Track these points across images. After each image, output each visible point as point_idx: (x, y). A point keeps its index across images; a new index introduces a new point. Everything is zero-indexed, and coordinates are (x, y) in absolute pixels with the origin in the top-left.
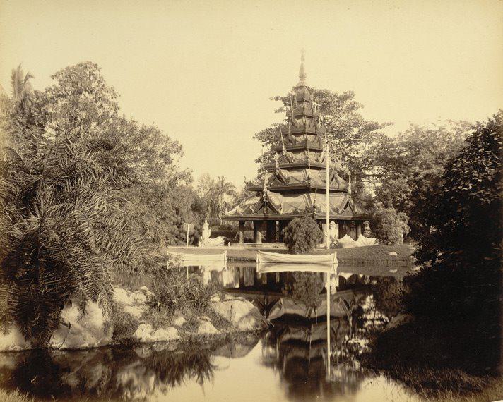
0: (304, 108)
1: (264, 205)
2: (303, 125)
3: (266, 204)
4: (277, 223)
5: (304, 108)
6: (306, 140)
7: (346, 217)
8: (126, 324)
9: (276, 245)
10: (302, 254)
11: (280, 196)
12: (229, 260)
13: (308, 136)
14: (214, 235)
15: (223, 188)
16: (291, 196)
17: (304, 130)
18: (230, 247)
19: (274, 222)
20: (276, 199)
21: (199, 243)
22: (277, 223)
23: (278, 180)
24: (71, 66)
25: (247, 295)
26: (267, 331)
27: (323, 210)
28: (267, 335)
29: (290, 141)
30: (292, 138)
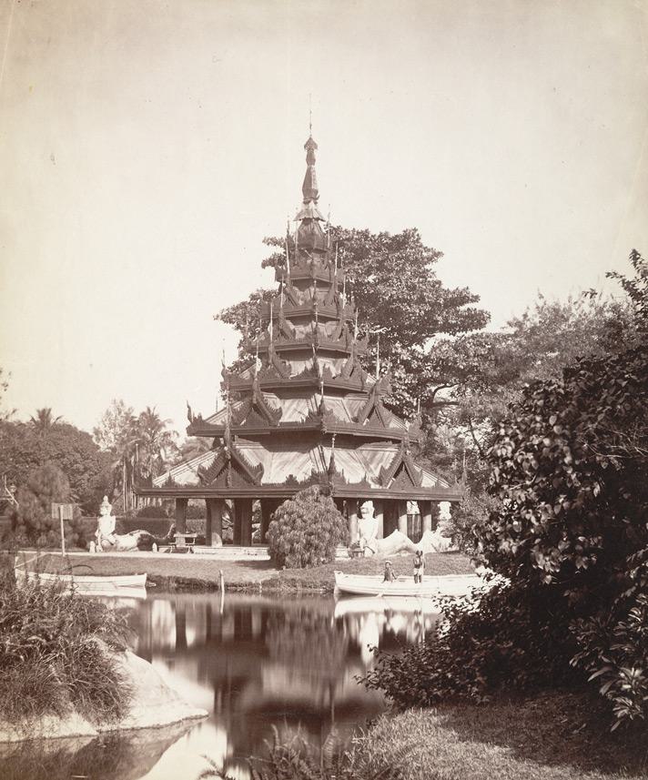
2: (346, 302)
3: (234, 463)
4: (257, 505)
7: (398, 494)
8: (578, 526)
9: (253, 550)
10: (191, 593)
11: (261, 449)
14: (124, 527)
16: (291, 450)
17: (312, 312)
18: (157, 553)
19: (250, 501)
20: (251, 454)
21: (92, 544)
22: (257, 505)
23: (255, 414)
24: (375, 231)
25: (168, 660)
29: (283, 333)
30: (288, 327)
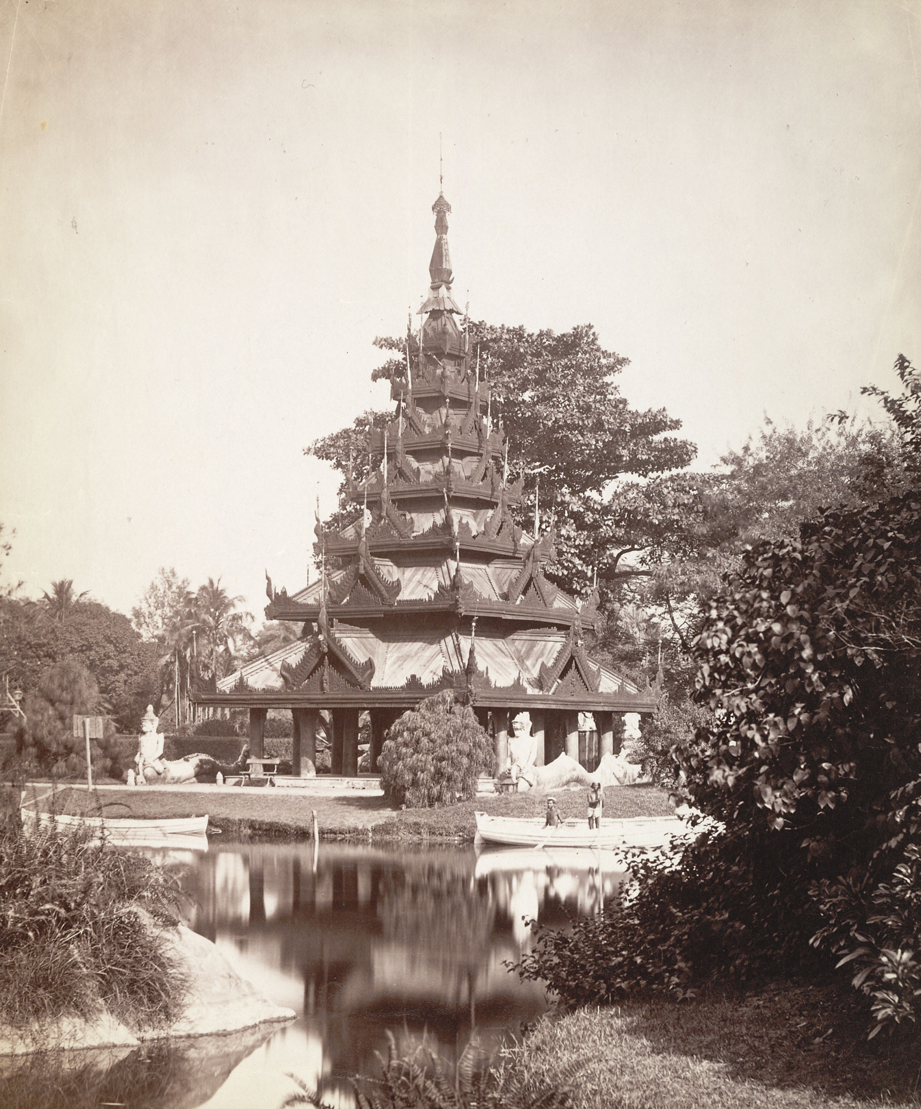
0: (443, 375)
1: (320, 663)
4: (365, 717)
5: (443, 375)
6: (448, 472)
7: (565, 702)
9: (359, 782)
11: (371, 639)
12: (210, 823)
13: (467, 568)
14: (177, 749)
15: (203, 610)
18: (223, 786)
20: (356, 645)
21: (131, 773)
22: (365, 717)
23: (363, 589)
25: (238, 938)
26: (766, 764)
27: (485, 596)
28: (749, 759)
29: (401, 473)
